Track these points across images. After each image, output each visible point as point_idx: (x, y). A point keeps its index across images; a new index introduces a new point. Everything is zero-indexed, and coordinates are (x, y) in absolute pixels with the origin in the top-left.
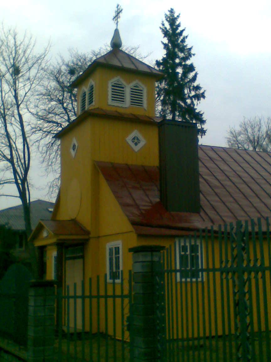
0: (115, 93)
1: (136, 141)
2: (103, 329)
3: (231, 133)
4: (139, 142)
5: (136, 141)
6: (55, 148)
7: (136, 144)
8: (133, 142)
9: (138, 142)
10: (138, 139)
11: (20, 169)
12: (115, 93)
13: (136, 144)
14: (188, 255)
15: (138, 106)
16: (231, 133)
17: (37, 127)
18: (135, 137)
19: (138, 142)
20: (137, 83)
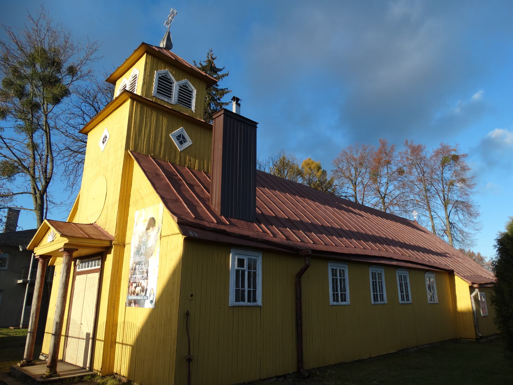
0: (189, 98)
1: (181, 139)
2: (125, 343)
3: (494, 246)
4: (185, 142)
5: (181, 139)
6: (150, 111)
7: (181, 143)
8: (178, 139)
9: (183, 141)
10: (183, 138)
11: (107, 113)
12: (189, 98)
13: (181, 143)
14: (342, 204)
15: (186, 62)
16: (494, 246)
17: (57, 121)
18: (181, 134)
19: (183, 141)
20: (186, 83)
